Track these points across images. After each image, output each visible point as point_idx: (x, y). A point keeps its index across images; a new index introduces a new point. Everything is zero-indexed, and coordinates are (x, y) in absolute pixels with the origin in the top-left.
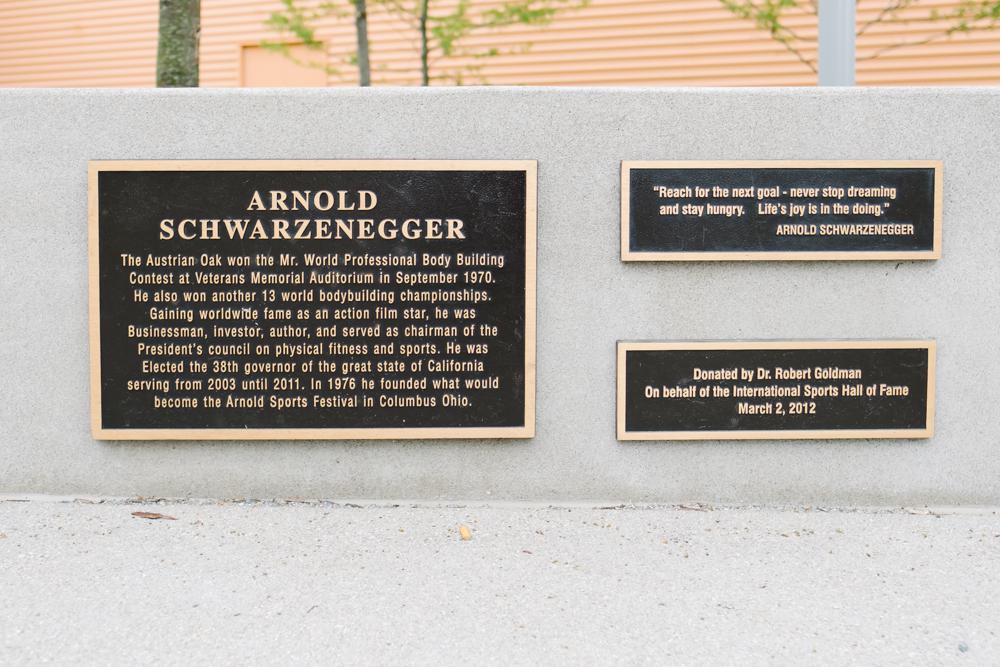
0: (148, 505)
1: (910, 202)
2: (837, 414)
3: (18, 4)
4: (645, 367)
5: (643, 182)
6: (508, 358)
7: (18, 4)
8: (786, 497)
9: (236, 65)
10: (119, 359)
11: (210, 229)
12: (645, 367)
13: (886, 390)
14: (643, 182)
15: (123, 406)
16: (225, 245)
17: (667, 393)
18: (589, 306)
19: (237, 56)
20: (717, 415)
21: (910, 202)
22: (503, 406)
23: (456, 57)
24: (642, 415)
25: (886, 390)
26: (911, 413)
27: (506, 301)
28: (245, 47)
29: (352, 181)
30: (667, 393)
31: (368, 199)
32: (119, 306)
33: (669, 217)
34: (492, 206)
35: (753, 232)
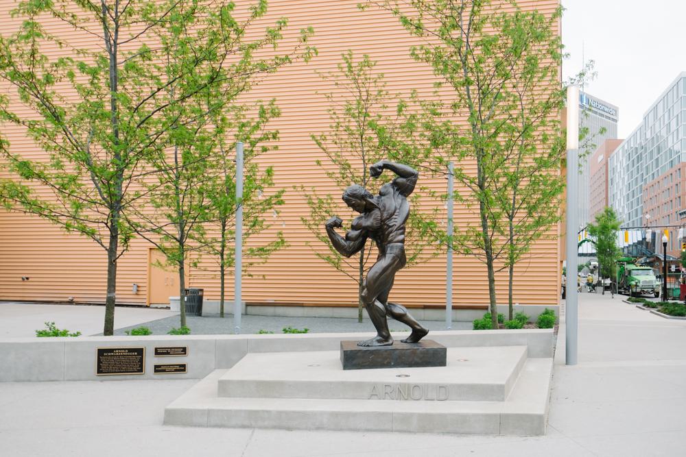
0: (102, 381)
1: (184, 350)
2: (176, 370)
3: (550, 2)
4: (156, 366)
5: (156, 349)
6: (141, 366)
7: (550, 2)
8: (171, 379)
9: (147, 257)
10: (99, 367)
11: (109, 354)
12: (156, 366)
13: (182, 368)
14: (156, 349)
15: (99, 371)
16: (111, 356)
17: (158, 369)
18: (150, 361)
19: (148, 252)
20: (164, 371)
21: (184, 350)
22: (141, 370)
23: (77, 61)
24: (156, 371)
25: (182, 368)
26: (184, 370)
27: (141, 361)
28: (151, 249)
29: (125, 349)
30: (158, 369)
31: (127, 351)
32: (99, 362)
33: (158, 352)
34: (140, 352)
35: (168, 353)
